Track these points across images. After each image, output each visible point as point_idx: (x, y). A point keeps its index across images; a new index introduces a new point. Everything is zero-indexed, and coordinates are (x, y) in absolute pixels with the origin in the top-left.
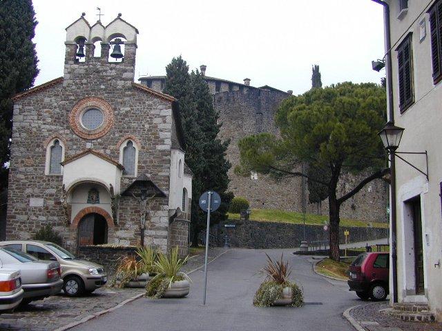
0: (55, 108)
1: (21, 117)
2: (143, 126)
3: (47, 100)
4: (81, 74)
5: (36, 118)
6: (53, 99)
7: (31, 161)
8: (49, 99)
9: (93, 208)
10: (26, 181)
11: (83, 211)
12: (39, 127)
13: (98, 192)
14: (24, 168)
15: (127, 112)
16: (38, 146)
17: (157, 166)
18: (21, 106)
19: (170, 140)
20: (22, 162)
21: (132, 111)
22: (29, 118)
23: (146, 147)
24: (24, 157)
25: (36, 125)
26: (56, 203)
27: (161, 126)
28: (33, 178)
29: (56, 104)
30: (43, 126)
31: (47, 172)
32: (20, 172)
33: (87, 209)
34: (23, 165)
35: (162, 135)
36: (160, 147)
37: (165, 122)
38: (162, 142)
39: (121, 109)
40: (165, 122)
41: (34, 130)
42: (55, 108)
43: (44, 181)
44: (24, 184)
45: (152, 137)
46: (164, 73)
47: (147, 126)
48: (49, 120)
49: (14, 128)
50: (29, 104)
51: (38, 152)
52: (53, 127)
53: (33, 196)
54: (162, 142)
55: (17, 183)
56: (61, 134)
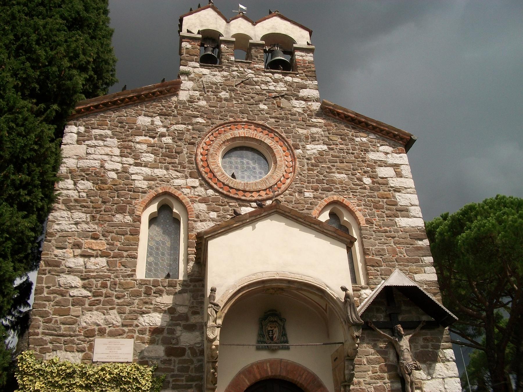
0: (163, 135)
1: (81, 149)
2: (360, 180)
3: (143, 121)
4: (215, 84)
5: (117, 152)
6: (157, 120)
7: (101, 245)
8: (149, 119)
9: (272, 363)
10: (86, 293)
11: (247, 371)
12: (125, 170)
13: (283, 320)
14: (81, 260)
15: (321, 153)
16: (121, 210)
17: (408, 261)
18: (82, 129)
19: (418, 209)
20: (77, 245)
21: (331, 152)
22: (100, 150)
23: (376, 220)
24: (84, 234)
25: (119, 167)
26: (169, 352)
27: (395, 182)
28: (104, 286)
29: (164, 130)
30: (133, 169)
31: (141, 274)
32: (71, 271)
33: (260, 365)
34: (78, 251)
35: (402, 199)
36: (403, 222)
37: (399, 175)
38: (404, 212)
39: (308, 147)
40: (399, 175)
41: (113, 175)
42: (163, 135)
43: (137, 295)
44: (78, 302)
45: (383, 202)
46: (108, 8)
47: (367, 181)
48: (150, 158)
49: (63, 169)
50: (100, 126)
51: (122, 224)
52: (160, 172)
53: (102, 332)
54: (404, 212)
55: (59, 298)
56: (179, 188)
